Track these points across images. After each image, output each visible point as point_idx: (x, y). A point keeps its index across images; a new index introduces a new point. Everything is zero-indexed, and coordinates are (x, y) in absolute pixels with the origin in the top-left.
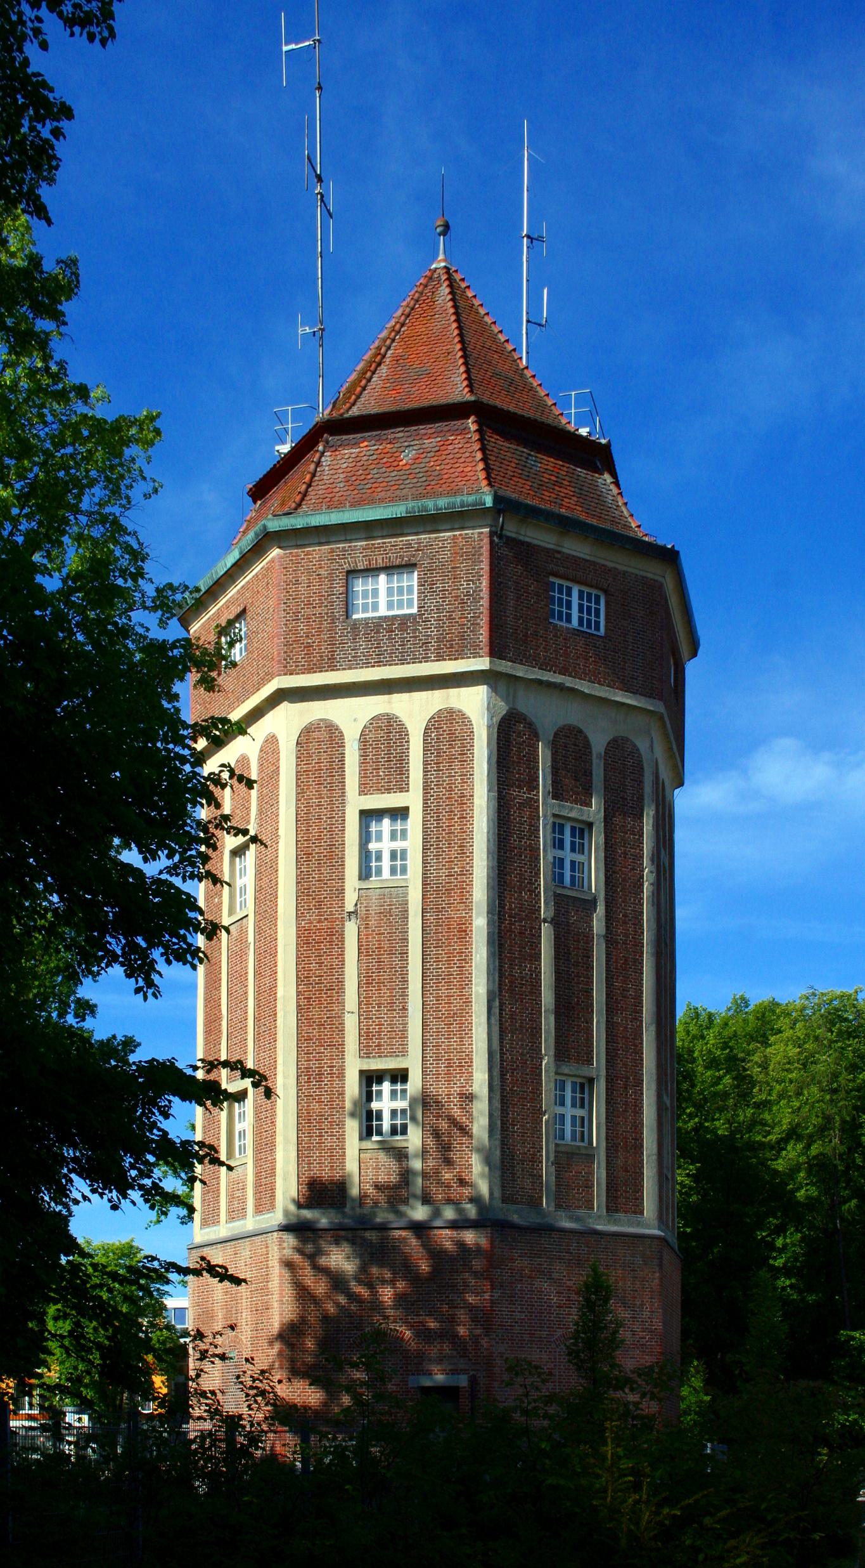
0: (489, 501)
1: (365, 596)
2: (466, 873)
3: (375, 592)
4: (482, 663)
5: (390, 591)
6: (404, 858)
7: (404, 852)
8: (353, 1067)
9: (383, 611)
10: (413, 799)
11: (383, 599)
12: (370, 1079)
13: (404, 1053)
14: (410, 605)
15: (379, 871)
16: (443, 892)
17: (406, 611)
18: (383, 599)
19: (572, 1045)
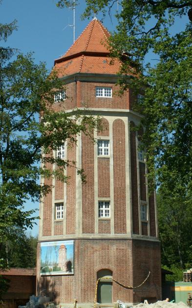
0: (166, 275)
1: (99, 92)
2: (118, 108)
3: (102, 92)
4: (128, 111)
5: (105, 92)
6: (108, 212)
7: (108, 211)
8: (97, 200)
9: (104, 96)
10: (110, 138)
11: (103, 93)
12: (101, 204)
13: (108, 135)
14: (110, 96)
15: (101, 153)
16: (118, 157)
17: (109, 97)
18: (103, 93)
19: (143, 198)
